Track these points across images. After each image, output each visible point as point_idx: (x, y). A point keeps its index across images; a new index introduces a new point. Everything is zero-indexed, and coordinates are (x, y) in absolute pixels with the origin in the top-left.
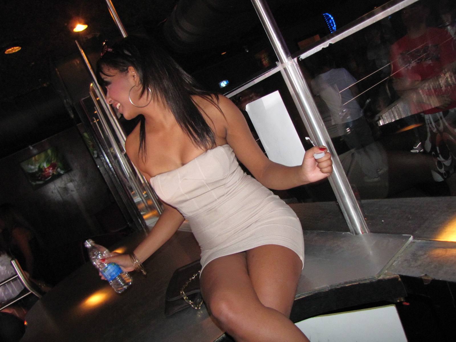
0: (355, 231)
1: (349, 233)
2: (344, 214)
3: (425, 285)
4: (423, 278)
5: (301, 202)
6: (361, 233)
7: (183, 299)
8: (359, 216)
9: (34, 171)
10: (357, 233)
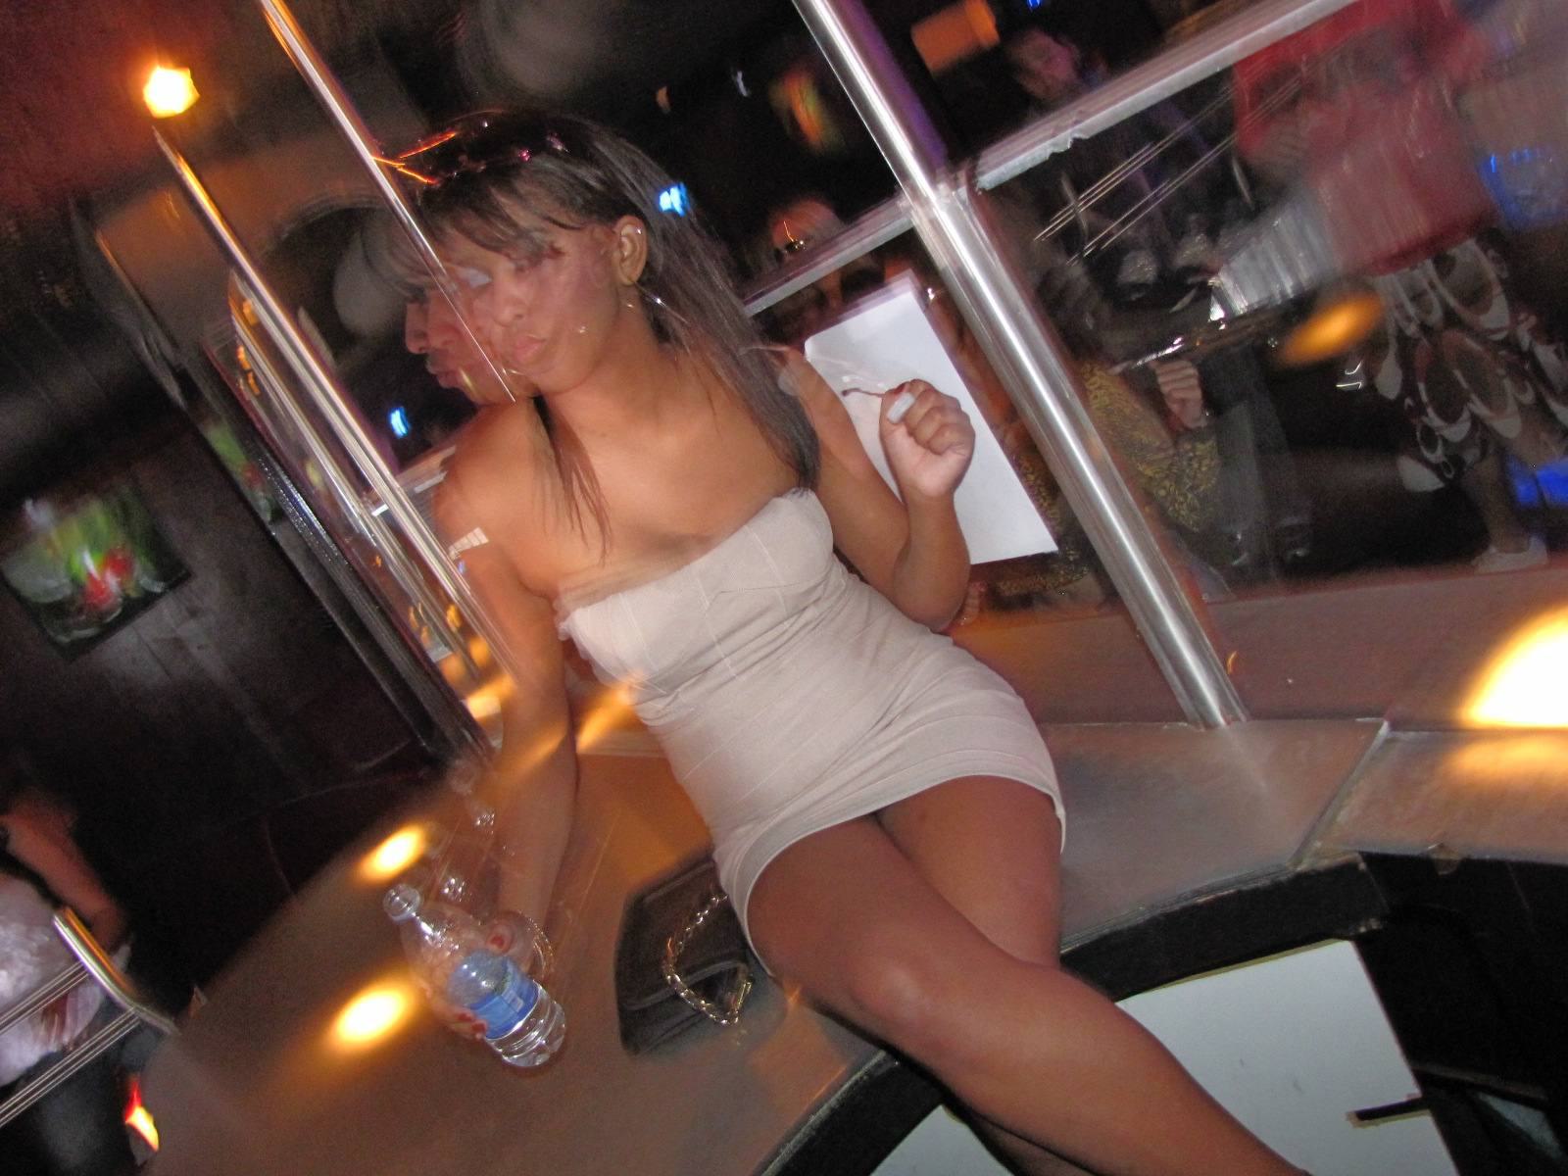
0: (1202, 716)
1: (1186, 725)
2: (1046, 458)
3: (1443, 876)
4: (1435, 856)
5: (1162, 915)
6: (1221, 720)
7: (676, 997)
8: (1212, 670)
9: (59, 597)
10: (1208, 723)
